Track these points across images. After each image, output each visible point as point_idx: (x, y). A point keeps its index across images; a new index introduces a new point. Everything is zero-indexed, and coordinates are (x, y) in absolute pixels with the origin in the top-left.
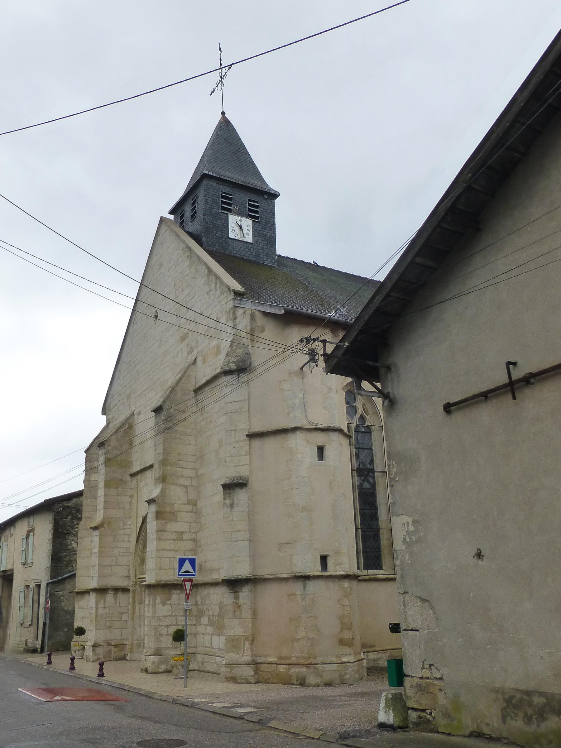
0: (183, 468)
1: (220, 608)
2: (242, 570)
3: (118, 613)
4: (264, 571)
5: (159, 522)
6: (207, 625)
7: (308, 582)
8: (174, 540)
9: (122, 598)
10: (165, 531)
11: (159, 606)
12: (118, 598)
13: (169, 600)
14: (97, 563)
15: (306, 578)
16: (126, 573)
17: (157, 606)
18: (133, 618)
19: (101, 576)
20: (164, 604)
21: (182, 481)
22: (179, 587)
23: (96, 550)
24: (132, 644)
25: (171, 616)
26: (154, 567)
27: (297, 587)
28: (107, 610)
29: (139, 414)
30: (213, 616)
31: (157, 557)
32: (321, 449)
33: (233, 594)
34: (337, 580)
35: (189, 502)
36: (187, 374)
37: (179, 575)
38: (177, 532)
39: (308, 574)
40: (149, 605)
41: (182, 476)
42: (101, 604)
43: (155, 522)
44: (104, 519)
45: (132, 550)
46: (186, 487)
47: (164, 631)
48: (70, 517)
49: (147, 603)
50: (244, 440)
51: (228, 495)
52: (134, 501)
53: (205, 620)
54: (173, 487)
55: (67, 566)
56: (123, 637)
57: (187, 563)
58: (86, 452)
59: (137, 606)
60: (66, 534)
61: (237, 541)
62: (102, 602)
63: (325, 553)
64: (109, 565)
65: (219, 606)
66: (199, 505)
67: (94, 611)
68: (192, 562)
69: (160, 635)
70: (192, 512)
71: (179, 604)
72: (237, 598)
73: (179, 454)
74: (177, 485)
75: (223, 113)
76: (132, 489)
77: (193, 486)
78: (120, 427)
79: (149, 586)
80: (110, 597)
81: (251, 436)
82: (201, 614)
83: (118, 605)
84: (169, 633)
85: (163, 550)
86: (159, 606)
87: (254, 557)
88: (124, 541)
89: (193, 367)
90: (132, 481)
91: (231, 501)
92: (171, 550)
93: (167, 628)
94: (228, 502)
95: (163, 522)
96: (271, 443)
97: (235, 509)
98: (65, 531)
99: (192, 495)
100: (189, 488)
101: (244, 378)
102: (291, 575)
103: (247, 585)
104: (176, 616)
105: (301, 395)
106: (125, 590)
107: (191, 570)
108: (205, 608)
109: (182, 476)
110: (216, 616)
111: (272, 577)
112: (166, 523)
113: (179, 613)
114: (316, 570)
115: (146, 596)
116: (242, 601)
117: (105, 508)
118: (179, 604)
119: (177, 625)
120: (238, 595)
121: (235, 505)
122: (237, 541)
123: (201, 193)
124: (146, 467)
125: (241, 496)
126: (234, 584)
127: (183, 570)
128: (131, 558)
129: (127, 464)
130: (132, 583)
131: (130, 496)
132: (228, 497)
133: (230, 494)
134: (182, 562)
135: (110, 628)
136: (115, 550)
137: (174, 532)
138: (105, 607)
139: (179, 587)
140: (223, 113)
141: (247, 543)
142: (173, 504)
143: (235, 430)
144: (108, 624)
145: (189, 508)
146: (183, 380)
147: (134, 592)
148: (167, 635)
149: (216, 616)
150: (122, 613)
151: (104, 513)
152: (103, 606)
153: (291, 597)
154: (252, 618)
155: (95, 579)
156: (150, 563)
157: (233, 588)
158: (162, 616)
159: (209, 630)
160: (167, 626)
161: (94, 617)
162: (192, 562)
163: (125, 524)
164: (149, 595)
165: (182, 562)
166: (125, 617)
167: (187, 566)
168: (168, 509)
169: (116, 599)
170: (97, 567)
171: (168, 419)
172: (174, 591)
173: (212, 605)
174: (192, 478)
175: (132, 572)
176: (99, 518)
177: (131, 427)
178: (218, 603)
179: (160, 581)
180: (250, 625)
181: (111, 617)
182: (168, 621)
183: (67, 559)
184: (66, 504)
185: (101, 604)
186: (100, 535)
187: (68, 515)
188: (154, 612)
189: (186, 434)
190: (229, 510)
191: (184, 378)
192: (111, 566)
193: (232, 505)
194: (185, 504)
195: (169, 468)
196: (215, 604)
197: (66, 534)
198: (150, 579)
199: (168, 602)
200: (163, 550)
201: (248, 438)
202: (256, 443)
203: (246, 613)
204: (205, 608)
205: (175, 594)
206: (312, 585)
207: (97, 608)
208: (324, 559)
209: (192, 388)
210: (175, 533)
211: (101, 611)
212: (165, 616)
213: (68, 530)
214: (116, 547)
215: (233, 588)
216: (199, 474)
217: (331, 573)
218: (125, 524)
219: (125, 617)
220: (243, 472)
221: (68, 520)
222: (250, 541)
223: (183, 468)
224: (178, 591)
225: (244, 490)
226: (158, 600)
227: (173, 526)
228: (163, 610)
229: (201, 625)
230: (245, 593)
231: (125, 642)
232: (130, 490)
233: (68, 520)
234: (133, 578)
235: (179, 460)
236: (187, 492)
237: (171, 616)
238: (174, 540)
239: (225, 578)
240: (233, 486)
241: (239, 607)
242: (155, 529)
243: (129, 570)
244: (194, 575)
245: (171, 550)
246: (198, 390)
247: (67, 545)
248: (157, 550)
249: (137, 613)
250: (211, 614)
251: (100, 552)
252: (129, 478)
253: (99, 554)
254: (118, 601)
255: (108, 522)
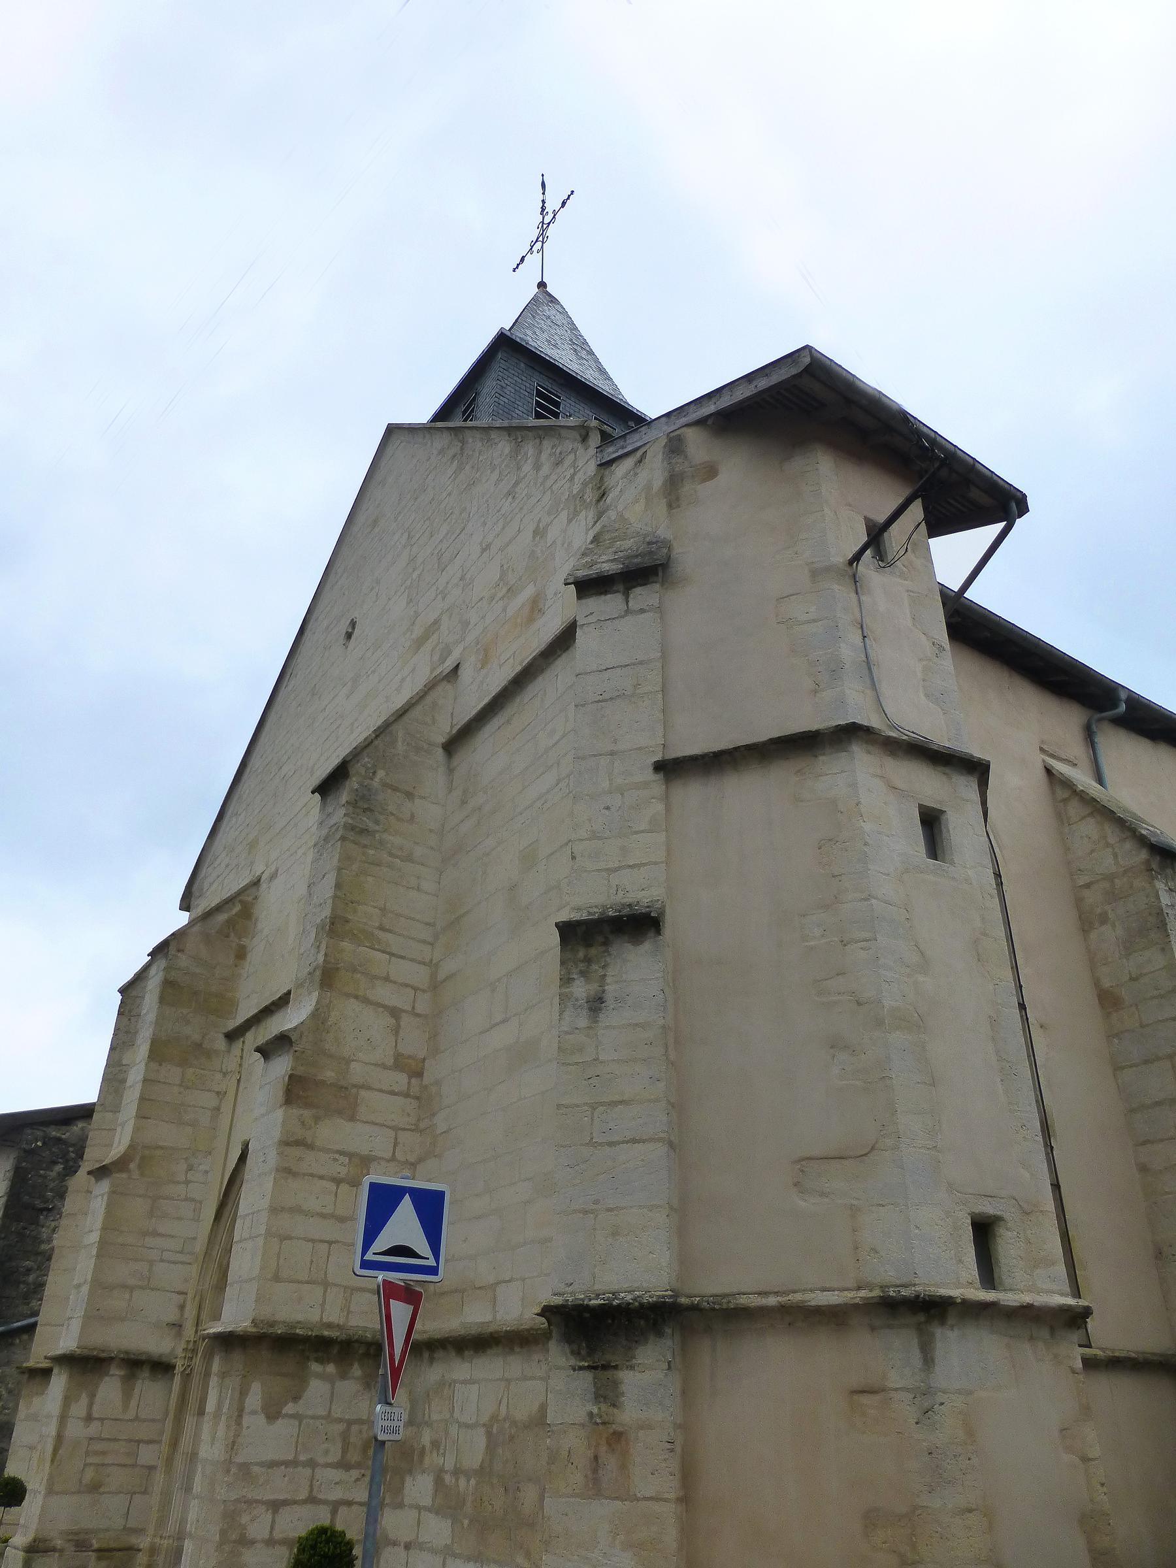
0: (392, 954)
1: (491, 1447)
2: (636, 1269)
3: (130, 1441)
4: (717, 1282)
5: (295, 1112)
6: (429, 1510)
7: (939, 1332)
8: (338, 1181)
9: (152, 1395)
10: (310, 1147)
11: (255, 1422)
12: (137, 1391)
13: (296, 1398)
14: (89, 1277)
15: (927, 1311)
16: (172, 1316)
17: (246, 1420)
18: (169, 1461)
19: (93, 1316)
20: (272, 1413)
21: (385, 994)
22: (335, 1350)
23: (94, 1237)
24: (153, 1550)
25: (294, 1463)
26: (256, 1272)
27: (889, 1355)
28: (94, 1429)
29: (273, 876)
30: (457, 1472)
31: (269, 1234)
32: (931, 821)
33: (588, 1376)
34: (1045, 1333)
35: (399, 1063)
36: (429, 699)
37: (365, 1265)
38: (350, 1155)
39: (943, 1292)
40: (217, 1414)
41: (387, 979)
42: (79, 1409)
43: (279, 1114)
44: (130, 1146)
45: (199, 1247)
46: (395, 1012)
47: (258, 1526)
48: (59, 1168)
49: (210, 1406)
50: (646, 785)
51: (582, 966)
52: (227, 1107)
53: (419, 1488)
54: (353, 1004)
55: (26, 1298)
56: (131, 1524)
57: (406, 1209)
58: (122, 991)
59: (190, 1421)
60: (41, 1210)
61: (611, 1144)
62: (84, 1400)
63: (988, 1208)
64: (124, 1286)
65: (489, 1434)
66: (428, 1078)
67: (52, 1430)
68: (430, 1208)
69: (245, 1542)
70: (407, 1095)
71: (328, 1417)
72: (607, 1394)
73: (383, 910)
74: (366, 1001)
75: (542, 285)
76: (225, 1074)
77: (418, 1015)
78: (218, 908)
79: (228, 1342)
80: (110, 1388)
81: (671, 769)
82: (409, 1457)
83: (131, 1414)
84: (278, 1535)
85: (297, 1210)
86: (255, 1422)
87: (684, 1212)
88: (180, 1219)
89: (445, 688)
90: (229, 1051)
91: (594, 987)
92: (323, 1216)
93: (281, 1241)
94: (581, 989)
95: (307, 1113)
96: (747, 795)
97: (605, 1019)
98: (38, 1204)
99: (413, 1042)
100: (405, 1020)
101: (642, 596)
102: (863, 1293)
103: (660, 1334)
104: (312, 1464)
105: (857, 638)
106: (161, 1367)
107: (420, 1244)
108: (426, 1438)
109: (387, 979)
110: (467, 1474)
111: (772, 1301)
112: (317, 1119)
113: (327, 1452)
114: (959, 1279)
115: (214, 1381)
116: (629, 1414)
117: (141, 1116)
118: (328, 1417)
119: (312, 1500)
120: (616, 1384)
121: (610, 1002)
122: (611, 1144)
123: (489, 386)
124: (273, 1003)
125: (634, 969)
126: (595, 1330)
127: (383, 1241)
128: (194, 1270)
129: (221, 1003)
130: (183, 1345)
131: (218, 1093)
132: (583, 974)
133: (588, 960)
134: (383, 1202)
135: (95, 1488)
136: (150, 1241)
137: (341, 1153)
138: (89, 1418)
139: (335, 1350)
140: (542, 285)
141: (658, 1151)
142: (348, 1062)
143: (612, 753)
144: (89, 1474)
145: (400, 1080)
146: (416, 713)
147: (187, 1376)
148: (270, 1542)
149: (467, 1474)
150: (139, 1442)
151: (136, 1130)
152: (83, 1413)
153: (865, 1399)
154: (679, 1500)
155: (76, 1326)
156: (245, 1262)
157: (591, 1351)
158: (262, 1464)
159: (437, 1530)
160: (276, 1506)
161: (49, 1449)
162: (430, 1208)
163: (190, 1168)
164: (223, 1375)
165: (383, 1202)
166: (147, 1455)
167: (404, 1227)
168: (329, 1075)
169: (127, 1395)
170: (85, 1289)
171: (363, 803)
172: (315, 1367)
173: (454, 1430)
174: (416, 989)
175: (190, 1312)
176: (117, 1150)
177: (247, 913)
178: (485, 1419)
179: (272, 1324)
180: (671, 1536)
181: (104, 1453)
182: (278, 1486)
183: (31, 1278)
184: (54, 1132)
185: (79, 1409)
186: (113, 1192)
187: (55, 1163)
188: (232, 1446)
189: (409, 858)
190: (583, 1022)
191: (419, 708)
192: (132, 1289)
193: (596, 1004)
194: (384, 1067)
195: (346, 945)
196: (468, 1426)
197: (41, 1210)
198: (235, 1316)
199: (290, 1408)
200: (297, 1210)
201: (660, 776)
202: (693, 794)
203: (652, 1473)
204: (426, 1438)
205: (320, 1376)
206: (962, 1353)
207: (63, 1418)
208: (984, 1230)
209: (442, 739)
210: (342, 1159)
211: (75, 1429)
212: (273, 1464)
213: (46, 1201)
214: (155, 1234)
215: (591, 1351)
216: (441, 976)
217: (1027, 1298)
218: (190, 1168)
219: (147, 1455)
220: (638, 890)
221: (53, 1174)
222: (671, 1145)
223: (392, 954)
224: (331, 1368)
225: (647, 946)
226: (254, 1399)
227: (335, 1133)
228: (268, 1439)
229: (400, 1506)
230: (647, 1377)
231: (134, 1540)
232: (219, 1076)
233: (53, 1174)
234: (189, 1332)
235: (382, 928)
236: (396, 1031)
237: (294, 1463)
238: (338, 1181)
239: (558, 1300)
240: (604, 934)
241: (617, 1439)
242: (277, 1134)
243: (182, 1307)
244: (433, 1271)
245: (323, 1216)
246: (454, 744)
247: (37, 1240)
248: (275, 1210)
249: (185, 1443)
250: (449, 1465)
251: (103, 1243)
252: (221, 1043)
253: (100, 1249)
254: (133, 1403)
255: (143, 1158)
